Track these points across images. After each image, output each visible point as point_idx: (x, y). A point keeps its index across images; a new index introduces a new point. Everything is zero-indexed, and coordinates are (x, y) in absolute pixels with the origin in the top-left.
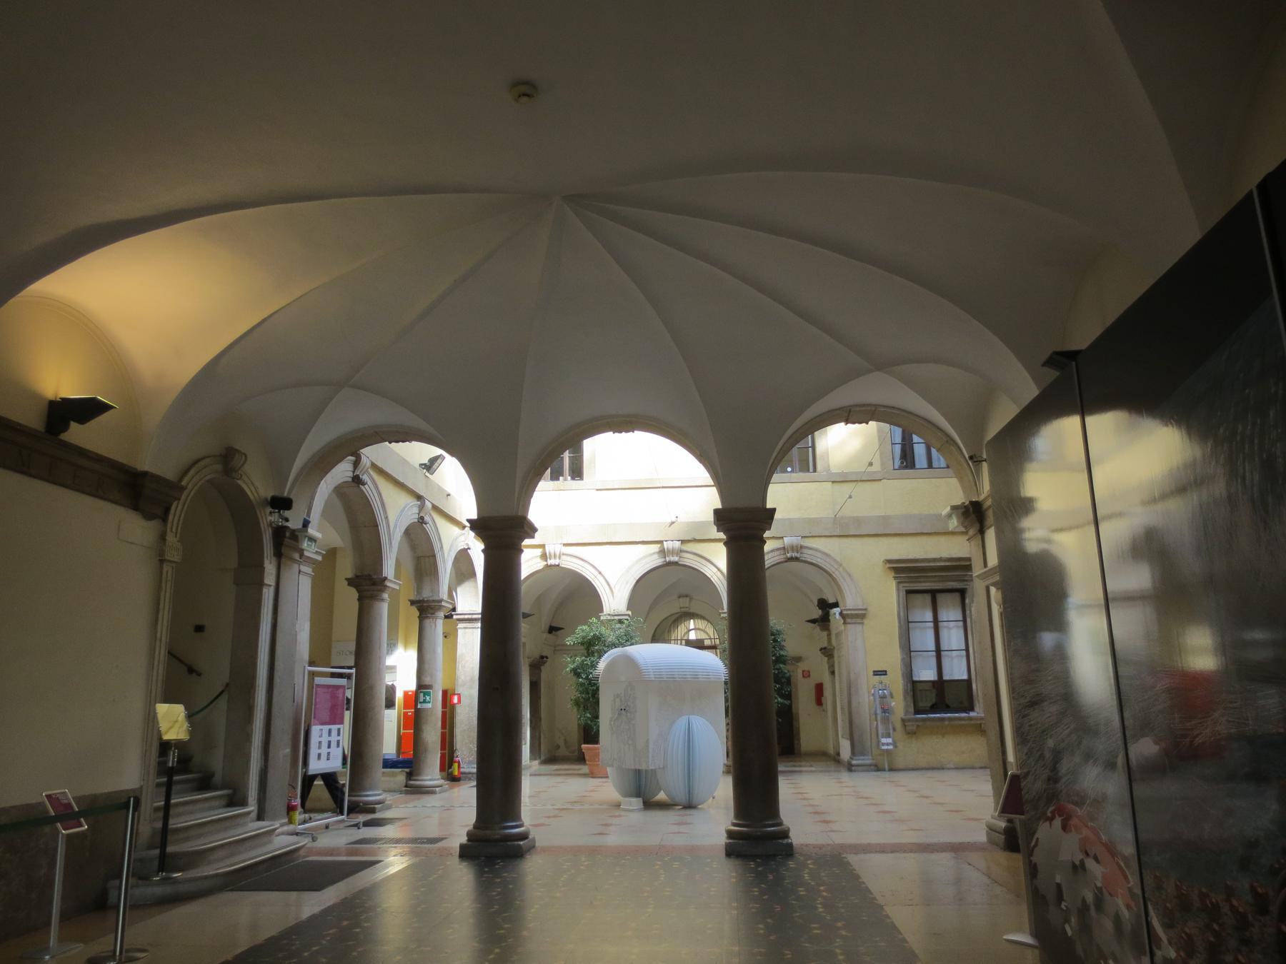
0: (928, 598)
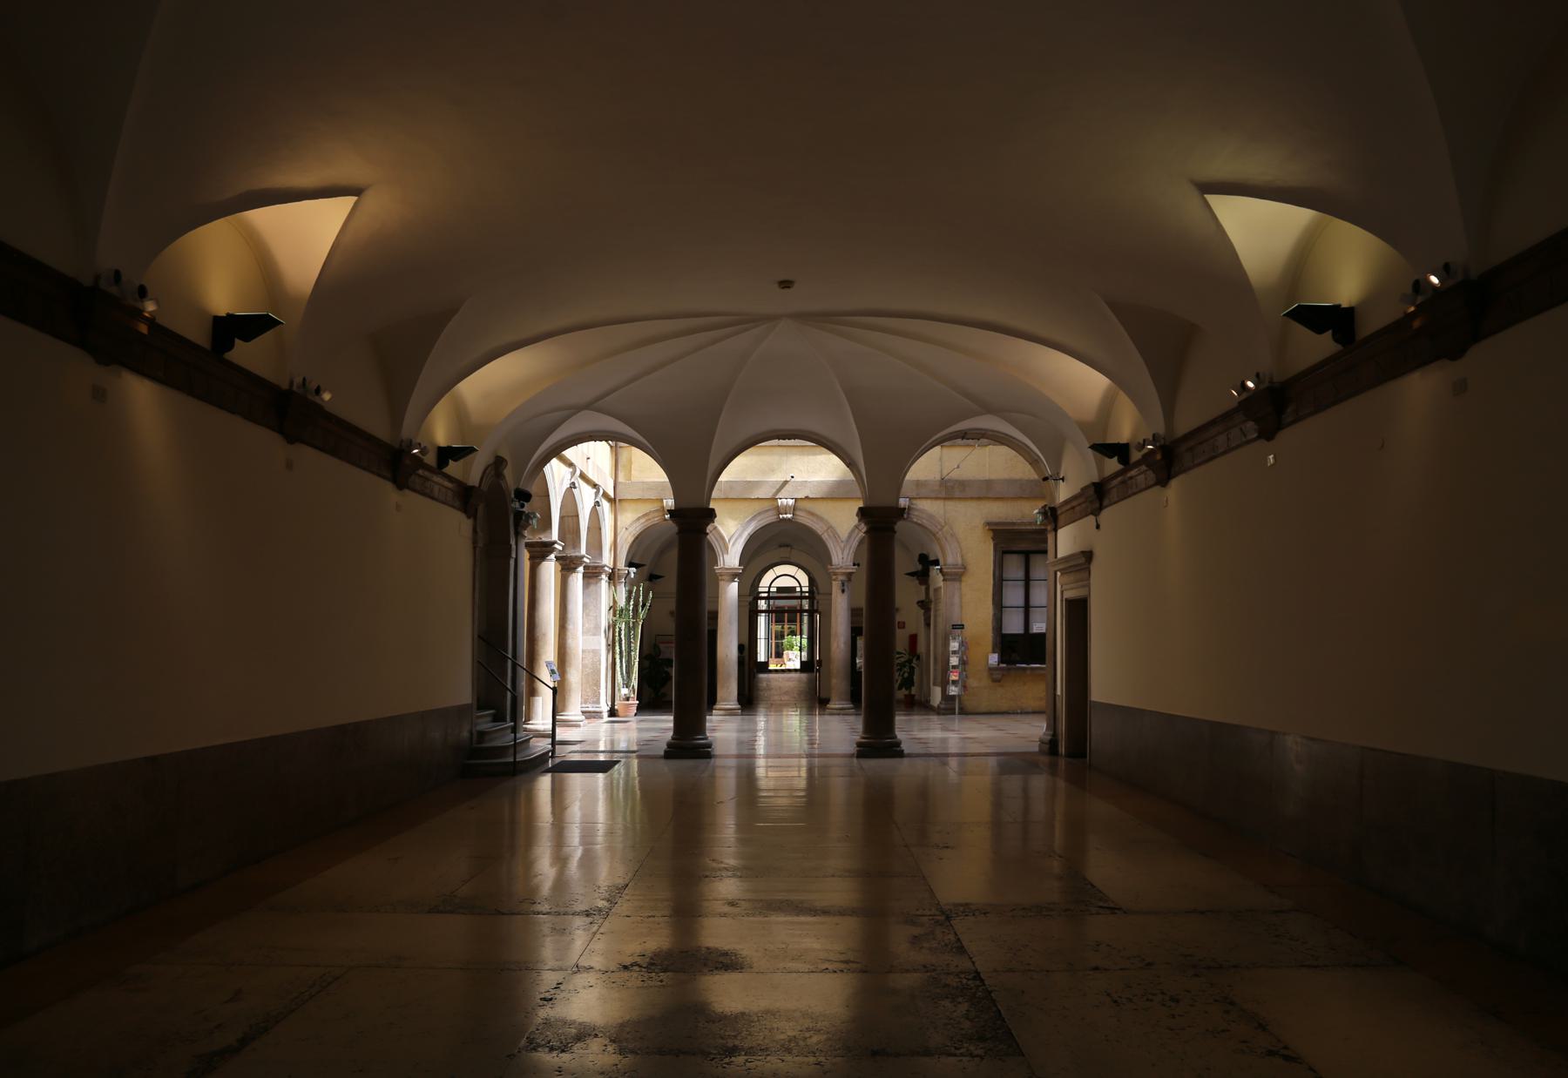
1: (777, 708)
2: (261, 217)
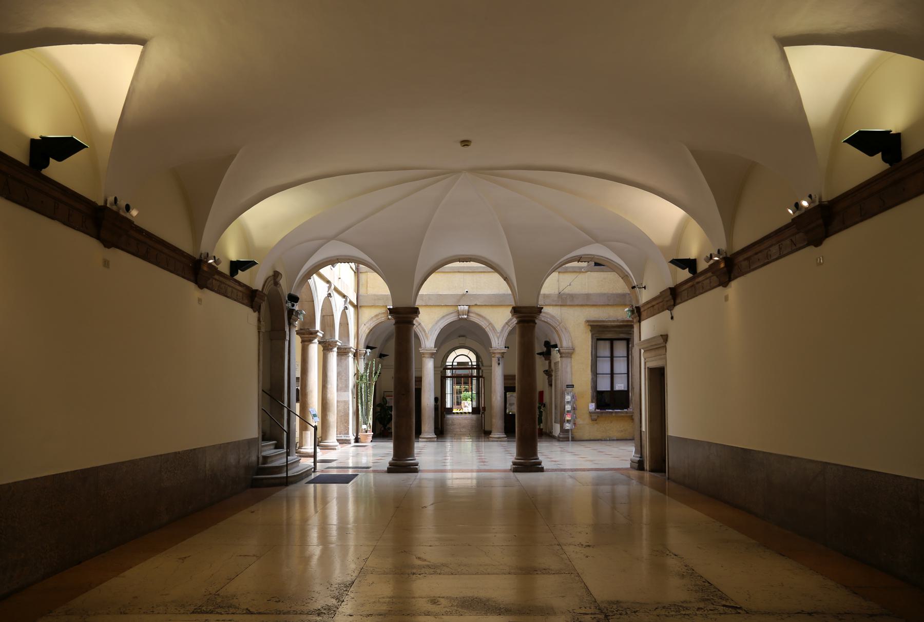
0: (608, 344)
1: (458, 436)
2: (63, 53)
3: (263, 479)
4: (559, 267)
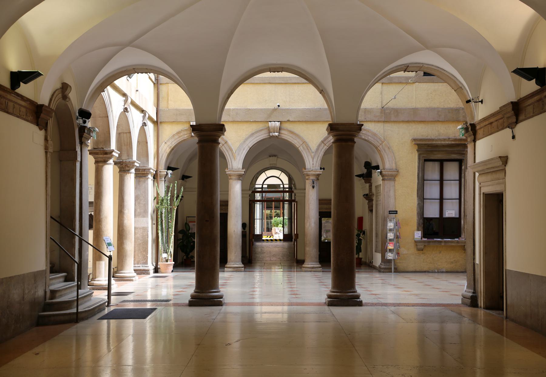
0: (437, 165)
1: (268, 266)
3: (54, 315)
4: (383, 77)
